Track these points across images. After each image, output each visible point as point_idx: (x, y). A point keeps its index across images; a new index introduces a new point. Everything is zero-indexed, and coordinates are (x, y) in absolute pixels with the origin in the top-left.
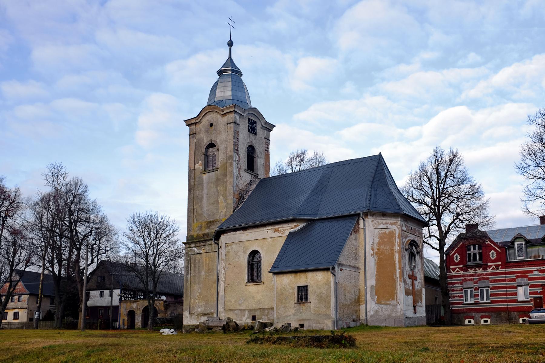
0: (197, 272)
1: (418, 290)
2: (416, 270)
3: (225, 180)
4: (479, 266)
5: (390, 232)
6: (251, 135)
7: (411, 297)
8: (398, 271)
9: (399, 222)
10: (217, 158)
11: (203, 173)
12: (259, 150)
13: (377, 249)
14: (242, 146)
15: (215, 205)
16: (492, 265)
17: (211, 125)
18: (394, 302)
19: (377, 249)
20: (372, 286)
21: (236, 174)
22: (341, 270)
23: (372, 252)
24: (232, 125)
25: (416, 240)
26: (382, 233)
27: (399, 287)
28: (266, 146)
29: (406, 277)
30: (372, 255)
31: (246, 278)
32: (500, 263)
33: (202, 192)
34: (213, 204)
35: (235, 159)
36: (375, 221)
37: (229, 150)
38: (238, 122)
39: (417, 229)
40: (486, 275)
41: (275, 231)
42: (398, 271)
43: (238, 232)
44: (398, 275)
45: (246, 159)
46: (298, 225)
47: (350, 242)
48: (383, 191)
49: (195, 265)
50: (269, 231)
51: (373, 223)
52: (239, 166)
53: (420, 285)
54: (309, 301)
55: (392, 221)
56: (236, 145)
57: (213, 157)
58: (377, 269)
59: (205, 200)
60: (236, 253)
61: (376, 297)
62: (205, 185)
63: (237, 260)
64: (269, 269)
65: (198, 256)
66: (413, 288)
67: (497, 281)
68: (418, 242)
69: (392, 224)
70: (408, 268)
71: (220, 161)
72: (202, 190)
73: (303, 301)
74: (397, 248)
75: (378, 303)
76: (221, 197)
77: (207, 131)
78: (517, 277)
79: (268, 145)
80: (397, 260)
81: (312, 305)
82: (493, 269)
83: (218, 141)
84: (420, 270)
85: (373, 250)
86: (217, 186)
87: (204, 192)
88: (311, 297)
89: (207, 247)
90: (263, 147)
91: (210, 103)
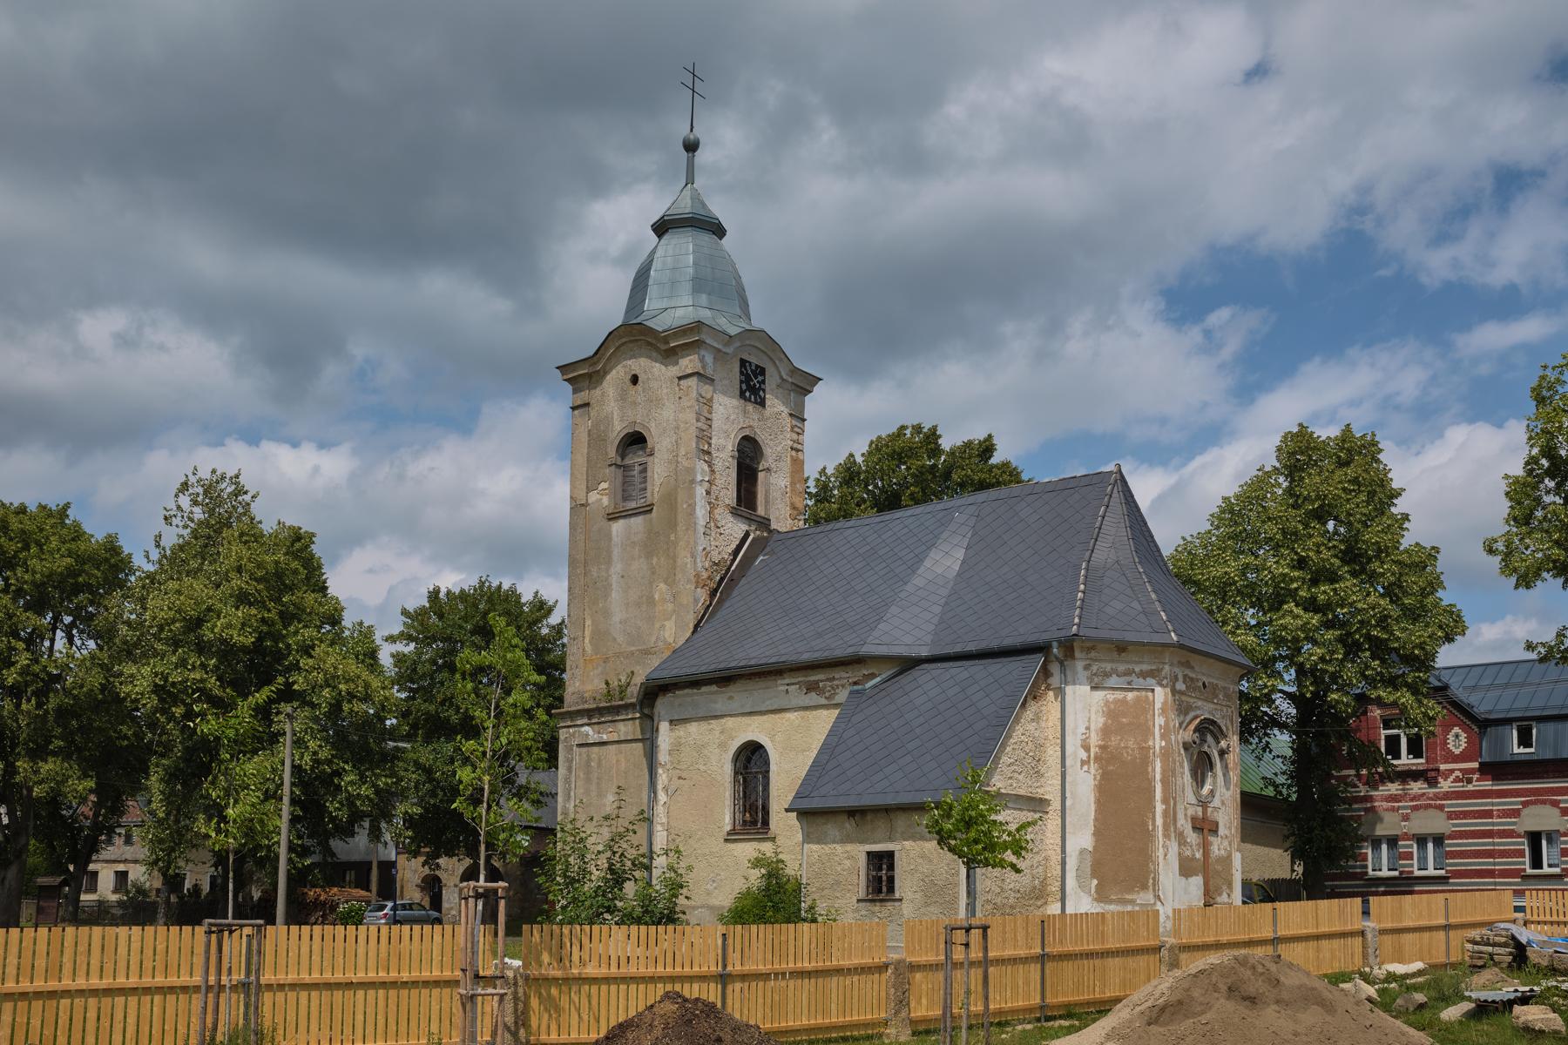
0: (594, 794)
1: (1220, 860)
2: (1216, 802)
4: (1414, 775)
5: (1138, 699)
6: (750, 407)
7: (1197, 882)
8: (1160, 808)
9: (1167, 667)
11: (612, 517)
12: (774, 450)
13: (1100, 747)
14: (722, 441)
16: (1452, 771)
17: (635, 380)
18: (1145, 897)
19: (1100, 747)
20: (1082, 851)
21: (702, 522)
23: (1084, 755)
24: (693, 381)
26: (1116, 701)
27: (1161, 853)
28: (795, 437)
30: (1083, 763)
31: (728, 819)
32: (1475, 765)
33: (607, 570)
35: (699, 478)
36: (1094, 668)
38: (709, 372)
39: (1221, 683)
40: (1436, 797)
41: (809, 690)
42: (1160, 808)
43: (704, 689)
44: (1159, 821)
45: (734, 475)
46: (873, 676)
47: (1024, 731)
50: (791, 688)
51: (1087, 673)
53: (1226, 843)
54: (897, 895)
55: (1145, 667)
56: (704, 436)
58: (1098, 802)
59: (615, 595)
61: (1095, 882)
62: (616, 552)
63: (702, 768)
65: (595, 749)
66: (1206, 854)
67: (1465, 815)
70: (1191, 798)
72: (609, 562)
74: (1158, 743)
75: (1101, 896)
76: (662, 586)
77: (622, 397)
78: (1525, 804)
80: (1158, 777)
81: (907, 909)
82: (1457, 780)
85: (1087, 748)
86: (649, 555)
87: (612, 570)
89: (621, 726)
90: (787, 439)
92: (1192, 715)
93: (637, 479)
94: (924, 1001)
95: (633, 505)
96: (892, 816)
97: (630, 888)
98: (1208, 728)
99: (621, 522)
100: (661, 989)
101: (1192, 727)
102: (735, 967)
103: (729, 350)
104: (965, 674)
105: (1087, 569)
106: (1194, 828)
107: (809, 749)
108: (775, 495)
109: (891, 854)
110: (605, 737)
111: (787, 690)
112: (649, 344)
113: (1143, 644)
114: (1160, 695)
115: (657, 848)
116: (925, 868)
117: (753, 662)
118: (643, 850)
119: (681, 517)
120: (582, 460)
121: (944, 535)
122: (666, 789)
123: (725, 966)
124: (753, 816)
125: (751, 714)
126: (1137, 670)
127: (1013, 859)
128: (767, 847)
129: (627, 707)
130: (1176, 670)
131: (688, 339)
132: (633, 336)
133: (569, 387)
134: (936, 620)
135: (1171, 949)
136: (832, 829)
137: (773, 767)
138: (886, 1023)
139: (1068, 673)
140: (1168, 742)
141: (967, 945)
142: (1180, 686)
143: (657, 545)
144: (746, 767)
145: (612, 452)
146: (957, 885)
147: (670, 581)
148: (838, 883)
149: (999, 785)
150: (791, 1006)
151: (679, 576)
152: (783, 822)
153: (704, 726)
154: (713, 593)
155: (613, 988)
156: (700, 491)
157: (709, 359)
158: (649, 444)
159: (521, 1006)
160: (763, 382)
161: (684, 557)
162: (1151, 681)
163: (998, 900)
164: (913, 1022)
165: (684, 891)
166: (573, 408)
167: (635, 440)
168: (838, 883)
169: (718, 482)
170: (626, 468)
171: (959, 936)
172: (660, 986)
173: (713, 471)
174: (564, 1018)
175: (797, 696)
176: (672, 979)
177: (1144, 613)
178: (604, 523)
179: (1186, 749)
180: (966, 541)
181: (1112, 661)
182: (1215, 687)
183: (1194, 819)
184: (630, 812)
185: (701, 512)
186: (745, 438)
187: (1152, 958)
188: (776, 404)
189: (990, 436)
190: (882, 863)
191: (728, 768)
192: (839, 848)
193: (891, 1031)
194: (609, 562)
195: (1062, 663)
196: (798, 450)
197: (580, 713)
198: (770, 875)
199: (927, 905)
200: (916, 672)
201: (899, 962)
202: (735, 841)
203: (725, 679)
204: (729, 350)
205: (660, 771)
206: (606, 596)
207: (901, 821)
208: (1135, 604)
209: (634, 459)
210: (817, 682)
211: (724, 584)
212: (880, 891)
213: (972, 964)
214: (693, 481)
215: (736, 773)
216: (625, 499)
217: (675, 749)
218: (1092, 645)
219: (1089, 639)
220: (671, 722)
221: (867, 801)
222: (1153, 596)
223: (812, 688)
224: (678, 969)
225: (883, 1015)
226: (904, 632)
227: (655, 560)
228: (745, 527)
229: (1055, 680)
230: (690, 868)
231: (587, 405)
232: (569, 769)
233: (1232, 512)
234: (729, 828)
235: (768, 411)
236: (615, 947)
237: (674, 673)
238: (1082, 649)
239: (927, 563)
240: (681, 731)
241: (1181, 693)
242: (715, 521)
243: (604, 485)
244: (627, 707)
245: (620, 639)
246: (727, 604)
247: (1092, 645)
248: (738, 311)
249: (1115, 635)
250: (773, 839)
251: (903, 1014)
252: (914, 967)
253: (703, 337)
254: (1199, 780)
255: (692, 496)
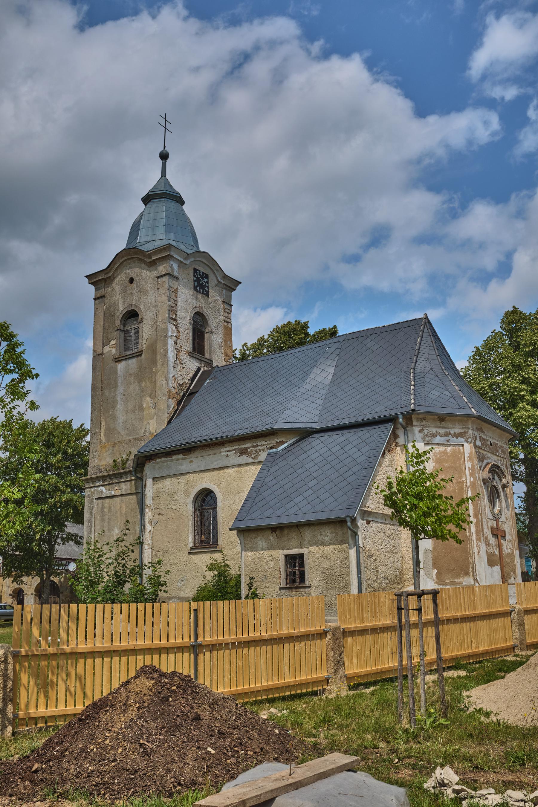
2: (503, 519)
3: (154, 369)
5: (454, 451)
6: (200, 296)
7: (497, 568)
9: (470, 431)
10: (140, 334)
11: (118, 360)
12: (214, 321)
14: (183, 314)
15: (137, 413)
17: (131, 281)
22: (368, 522)
24: (166, 279)
25: (499, 464)
26: (440, 453)
27: (476, 551)
28: (226, 315)
29: (488, 532)
31: (191, 539)
33: (115, 391)
34: (133, 411)
35: (170, 334)
36: (426, 432)
37: (160, 319)
38: (176, 274)
43: (174, 457)
45: (191, 334)
46: (282, 443)
48: (436, 378)
49: (102, 516)
50: (230, 453)
51: (421, 435)
52: (178, 345)
53: (510, 545)
54: (307, 584)
55: (457, 431)
56: (173, 310)
57: (135, 334)
59: (119, 406)
60: (172, 494)
61: (435, 571)
62: (120, 381)
63: (174, 507)
64: (230, 524)
65: (107, 501)
66: (500, 551)
68: (502, 467)
69: (457, 436)
71: (145, 338)
73: (296, 585)
76: (148, 399)
77: (124, 291)
79: (230, 313)
81: (314, 592)
83: (142, 306)
84: (509, 518)
86: (140, 381)
87: (118, 392)
88: (312, 577)
89: (123, 486)
90: (221, 316)
91: (128, 247)
92: (486, 462)
93: (133, 338)
94: (355, 661)
95: (131, 352)
96: (302, 530)
97: (127, 587)
98: (495, 470)
99: (123, 363)
100: (141, 661)
101: (487, 469)
102: (206, 638)
103: (188, 262)
104: (343, 439)
105: (414, 373)
106: (493, 534)
107: (242, 491)
108: (215, 346)
109: (301, 556)
110: (113, 493)
111: (228, 455)
112: (140, 259)
113: (456, 416)
114: (468, 448)
115: (146, 561)
116: (326, 564)
117: (205, 438)
118: (138, 562)
119: (159, 357)
120: (100, 329)
121: (321, 360)
122: (151, 522)
123: (196, 637)
124: (206, 538)
125: (204, 471)
126: (452, 432)
127: (454, 530)
128: (218, 556)
129: (126, 473)
130: (475, 433)
131: (164, 254)
132: (132, 255)
133: (93, 288)
134: (320, 408)
135: (519, 612)
136: (261, 542)
137: (219, 504)
138: (327, 680)
139: (409, 435)
140: (475, 478)
141: (419, 610)
142: (479, 443)
143: (146, 374)
144: (202, 506)
145: (118, 322)
146: (348, 575)
147: (153, 396)
148: (266, 577)
149: (372, 507)
150: (252, 670)
151: (158, 392)
152: (228, 539)
153: (175, 480)
154: (179, 403)
155: (98, 661)
156: (171, 342)
157: (175, 266)
158: (140, 317)
159: (10, 684)
160: (207, 282)
161: (161, 380)
162: (461, 440)
163: (375, 585)
164: (349, 679)
165: (164, 588)
166: (95, 299)
167: (132, 315)
168: (266, 577)
169: (181, 337)
170: (126, 332)
171: (413, 602)
172: (140, 657)
173: (178, 331)
174: (52, 694)
175: (234, 458)
176: (151, 651)
177: (453, 397)
178: (113, 364)
179: (484, 483)
180: (334, 364)
181: (436, 427)
182: (496, 445)
183: (492, 528)
184: (130, 539)
185: (171, 354)
186: (197, 313)
187: (507, 620)
188: (215, 296)
189: (335, 326)
190: (295, 563)
191: (190, 507)
192: (266, 553)
193: (332, 687)
194: (116, 387)
195: (405, 429)
196: (228, 322)
197: (98, 479)
198: (220, 575)
199: (328, 589)
200: (310, 439)
201: (336, 629)
202: (196, 553)
203: (187, 450)
204: (188, 262)
205: (147, 510)
206: (114, 407)
207: (308, 533)
208: (446, 393)
209: (131, 326)
210: (246, 449)
211: (186, 396)
212: (295, 582)
213: (425, 624)
214: (166, 336)
215: (195, 510)
216: (126, 349)
217: (157, 496)
218: (423, 416)
219: (422, 413)
220: (154, 478)
221: (284, 520)
222: (457, 388)
223: (243, 452)
224: (156, 642)
225: (325, 674)
226: (300, 414)
227: (144, 383)
228: (198, 365)
229: (401, 440)
230: (168, 572)
231: (103, 297)
232: (91, 514)
233: (480, 355)
234: (191, 545)
235: (210, 299)
236: (112, 624)
237: (155, 447)
238: (418, 419)
239: (312, 376)
240: (160, 485)
241: (479, 448)
242: (180, 360)
243: (113, 342)
244: (126, 473)
245: (123, 432)
246: (188, 408)
247: (423, 416)
248: (192, 243)
249: (438, 411)
250: (221, 551)
251: (341, 673)
252: (347, 633)
253: (172, 253)
254: (493, 505)
255: (166, 344)
